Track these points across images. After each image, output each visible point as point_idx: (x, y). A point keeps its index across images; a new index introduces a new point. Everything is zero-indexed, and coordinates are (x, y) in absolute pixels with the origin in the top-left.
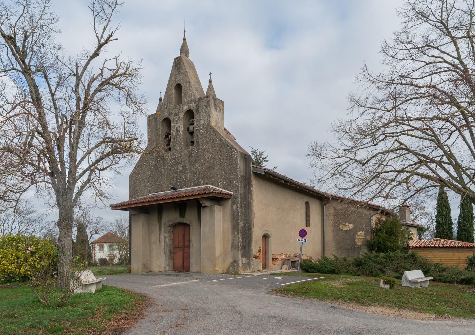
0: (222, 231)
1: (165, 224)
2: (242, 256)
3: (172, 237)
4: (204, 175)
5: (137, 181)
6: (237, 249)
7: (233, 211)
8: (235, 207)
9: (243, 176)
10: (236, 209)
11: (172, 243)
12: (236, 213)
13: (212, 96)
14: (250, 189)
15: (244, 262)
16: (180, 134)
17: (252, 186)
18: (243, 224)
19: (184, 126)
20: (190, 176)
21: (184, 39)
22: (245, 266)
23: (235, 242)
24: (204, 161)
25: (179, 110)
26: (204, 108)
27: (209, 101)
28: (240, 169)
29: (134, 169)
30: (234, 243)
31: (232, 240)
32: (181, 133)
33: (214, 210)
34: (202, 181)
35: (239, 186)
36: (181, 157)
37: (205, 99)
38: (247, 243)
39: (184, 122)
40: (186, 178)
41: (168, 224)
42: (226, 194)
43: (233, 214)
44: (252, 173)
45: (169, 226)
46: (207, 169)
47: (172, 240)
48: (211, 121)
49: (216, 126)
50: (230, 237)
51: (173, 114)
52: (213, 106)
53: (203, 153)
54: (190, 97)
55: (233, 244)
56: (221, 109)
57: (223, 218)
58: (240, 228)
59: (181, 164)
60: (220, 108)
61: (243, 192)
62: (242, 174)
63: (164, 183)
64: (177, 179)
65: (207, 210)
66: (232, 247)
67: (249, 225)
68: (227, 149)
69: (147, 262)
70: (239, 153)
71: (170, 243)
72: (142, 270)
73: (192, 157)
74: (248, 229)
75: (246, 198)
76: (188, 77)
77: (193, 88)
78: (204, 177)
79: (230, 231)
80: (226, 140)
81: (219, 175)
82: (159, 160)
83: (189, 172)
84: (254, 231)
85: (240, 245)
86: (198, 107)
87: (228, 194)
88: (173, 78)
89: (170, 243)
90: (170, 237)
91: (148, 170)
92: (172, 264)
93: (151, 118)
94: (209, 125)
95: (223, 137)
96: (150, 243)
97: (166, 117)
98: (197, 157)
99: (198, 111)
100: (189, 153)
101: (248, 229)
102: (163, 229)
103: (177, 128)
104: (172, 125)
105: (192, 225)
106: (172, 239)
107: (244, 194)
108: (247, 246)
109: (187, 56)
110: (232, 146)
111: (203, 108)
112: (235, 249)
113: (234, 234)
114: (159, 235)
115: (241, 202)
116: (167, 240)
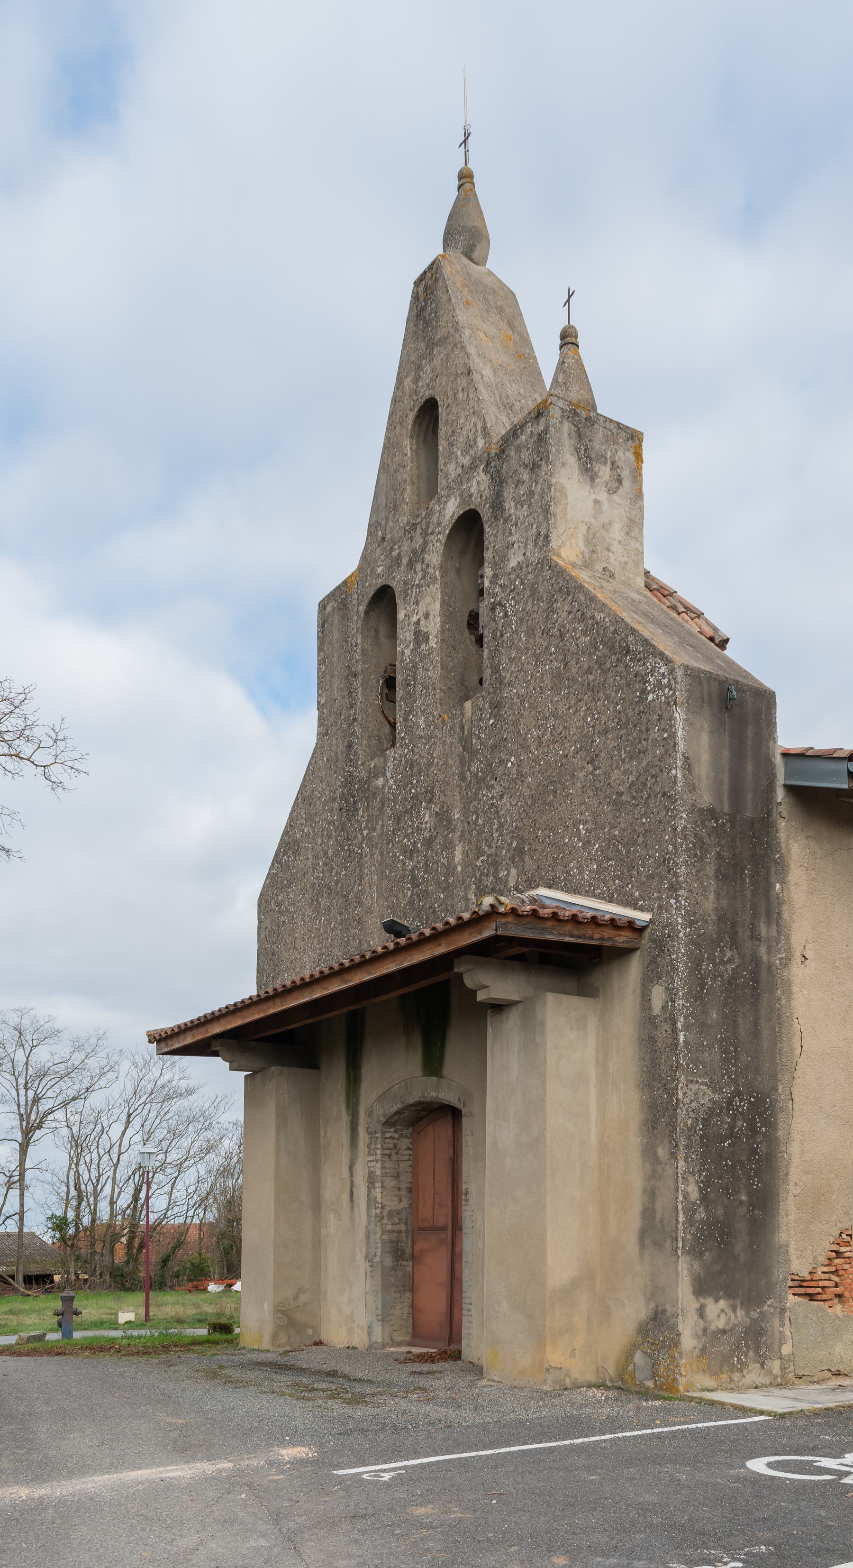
0: (593, 1139)
1: (370, 1114)
2: (701, 1288)
3: (406, 1180)
4: (522, 840)
5: (282, 919)
6: (668, 1243)
7: (648, 1021)
8: (658, 995)
9: (712, 813)
10: (664, 1008)
11: (405, 1204)
12: (663, 1032)
13: (560, 403)
14: (769, 887)
15: (721, 1324)
16: (430, 651)
17: (783, 869)
18: (707, 1096)
19: (443, 603)
20: (466, 854)
21: (465, 177)
22: (725, 1349)
23: (658, 1206)
24: (520, 764)
25: (425, 534)
26: (525, 477)
27: (546, 431)
28: (688, 765)
29: (273, 864)
30: (654, 1211)
31: (644, 1190)
32: (433, 643)
33: (542, 1024)
34: (513, 871)
35: (682, 871)
36: (430, 765)
37: (528, 429)
38: (742, 1210)
39: (445, 586)
40: (450, 870)
41: (381, 1112)
42: (594, 921)
43: (652, 1039)
44: (780, 794)
45: (389, 1123)
46: (534, 801)
47: (410, 1190)
48: (553, 537)
49: (587, 565)
50: (637, 1180)
51: (405, 561)
52: (571, 460)
53: (516, 723)
54: (470, 444)
55: (648, 1213)
56: (626, 474)
57: (602, 1064)
58: (684, 1118)
59: (430, 801)
60: (614, 466)
61: (709, 904)
62: (706, 799)
63: (370, 911)
64: (415, 882)
65: (512, 1021)
66: (643, 1234)
67: (760, 1101)
68: (621, 668)
69: (304, 1298)
70: (679, 673)
71: (393, 1204)
72: (275, 1336)
73: (473, 753)
74: (752, 1127)
75: (735, 944)
76: (463, 348)
77: (484, 394)
78: (520, 851)
79: (635, 1141)
80: (618, 621)
81: (585, 823)
82: (355, 802)
83: (462, 835)
84: (796, 1136)
85: (690, 1222)
86: (501, 482)
87: (613, 923)
88: (408, 382)
89: (393, 1204)
90: (397, 1176)
91: (316, 857)
92: (406, 1310)
93: (329, 609)
94: (546, 564)
95: (603, 607)
96: (317, 1205)
97: (380, 582)
98: (494, 747)
99: (497, 505)
100: (461, 740)
101: (752, 1127)
102: (363, 1138)
103: (418, 623)
104: (401, 615)
105: (471, 1114)
106: (404, 1186)
107: (721, 919)
108: (741, 1225)
109: (476, 255)
110: (646, 642)
111: (519, 483)
112: (659, 1245)
113: (655, 1154)
114: (351, 1168)
115: (696, 963)
116: (378, 1193)
